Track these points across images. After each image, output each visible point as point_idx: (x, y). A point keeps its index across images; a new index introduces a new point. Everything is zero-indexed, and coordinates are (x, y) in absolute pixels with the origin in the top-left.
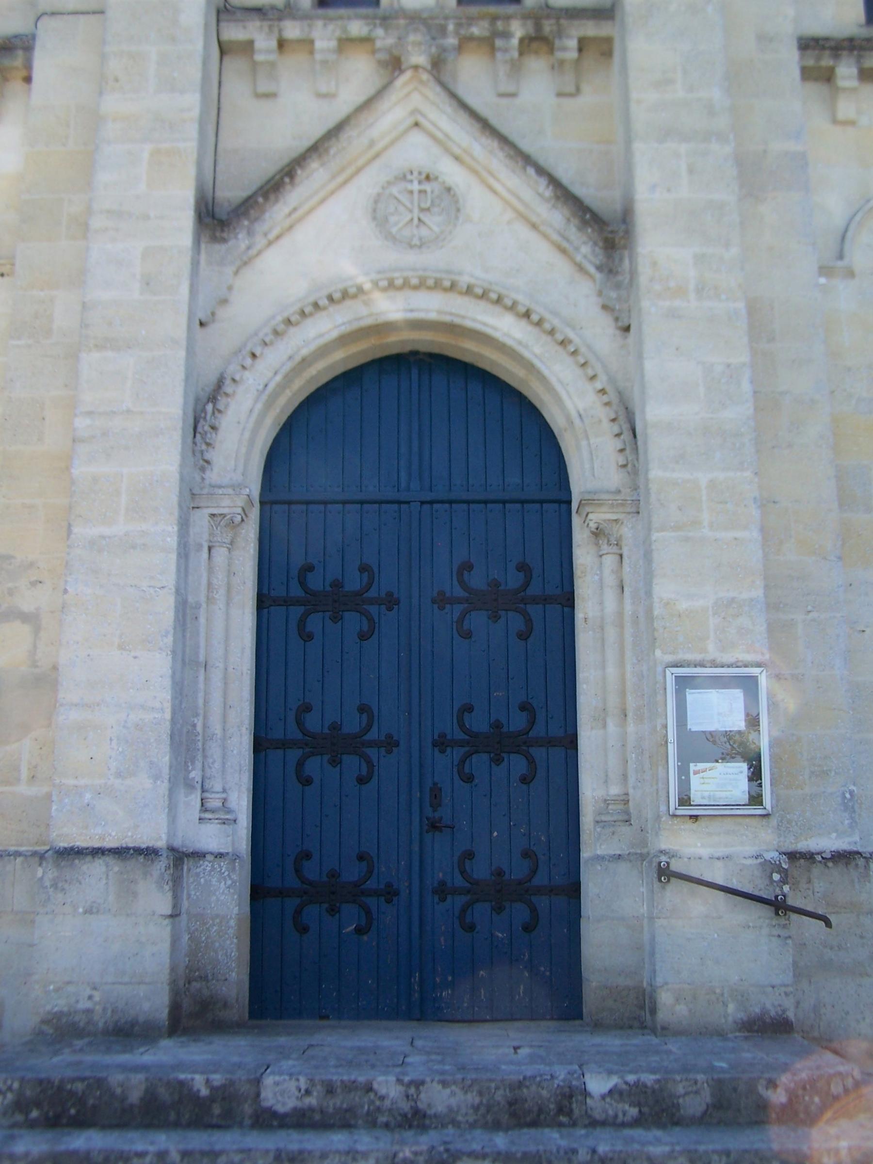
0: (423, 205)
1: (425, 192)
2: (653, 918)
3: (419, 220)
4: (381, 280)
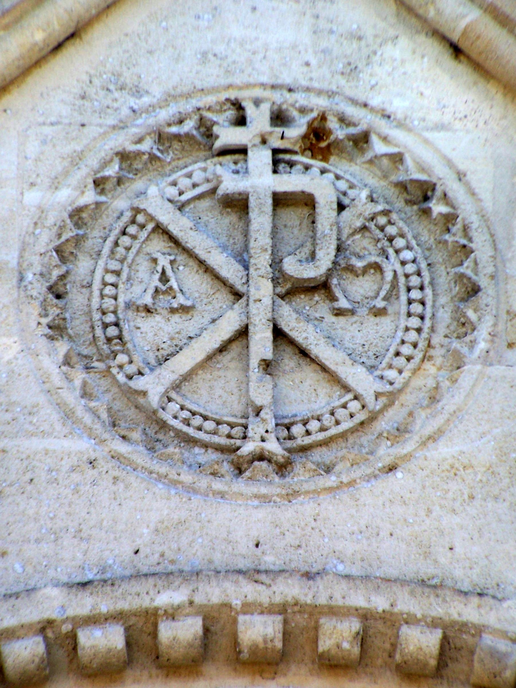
0: (294, 268)
1: (307, 201)
2: (161, 428)
3: (278, 334)
4: (93, 620)
